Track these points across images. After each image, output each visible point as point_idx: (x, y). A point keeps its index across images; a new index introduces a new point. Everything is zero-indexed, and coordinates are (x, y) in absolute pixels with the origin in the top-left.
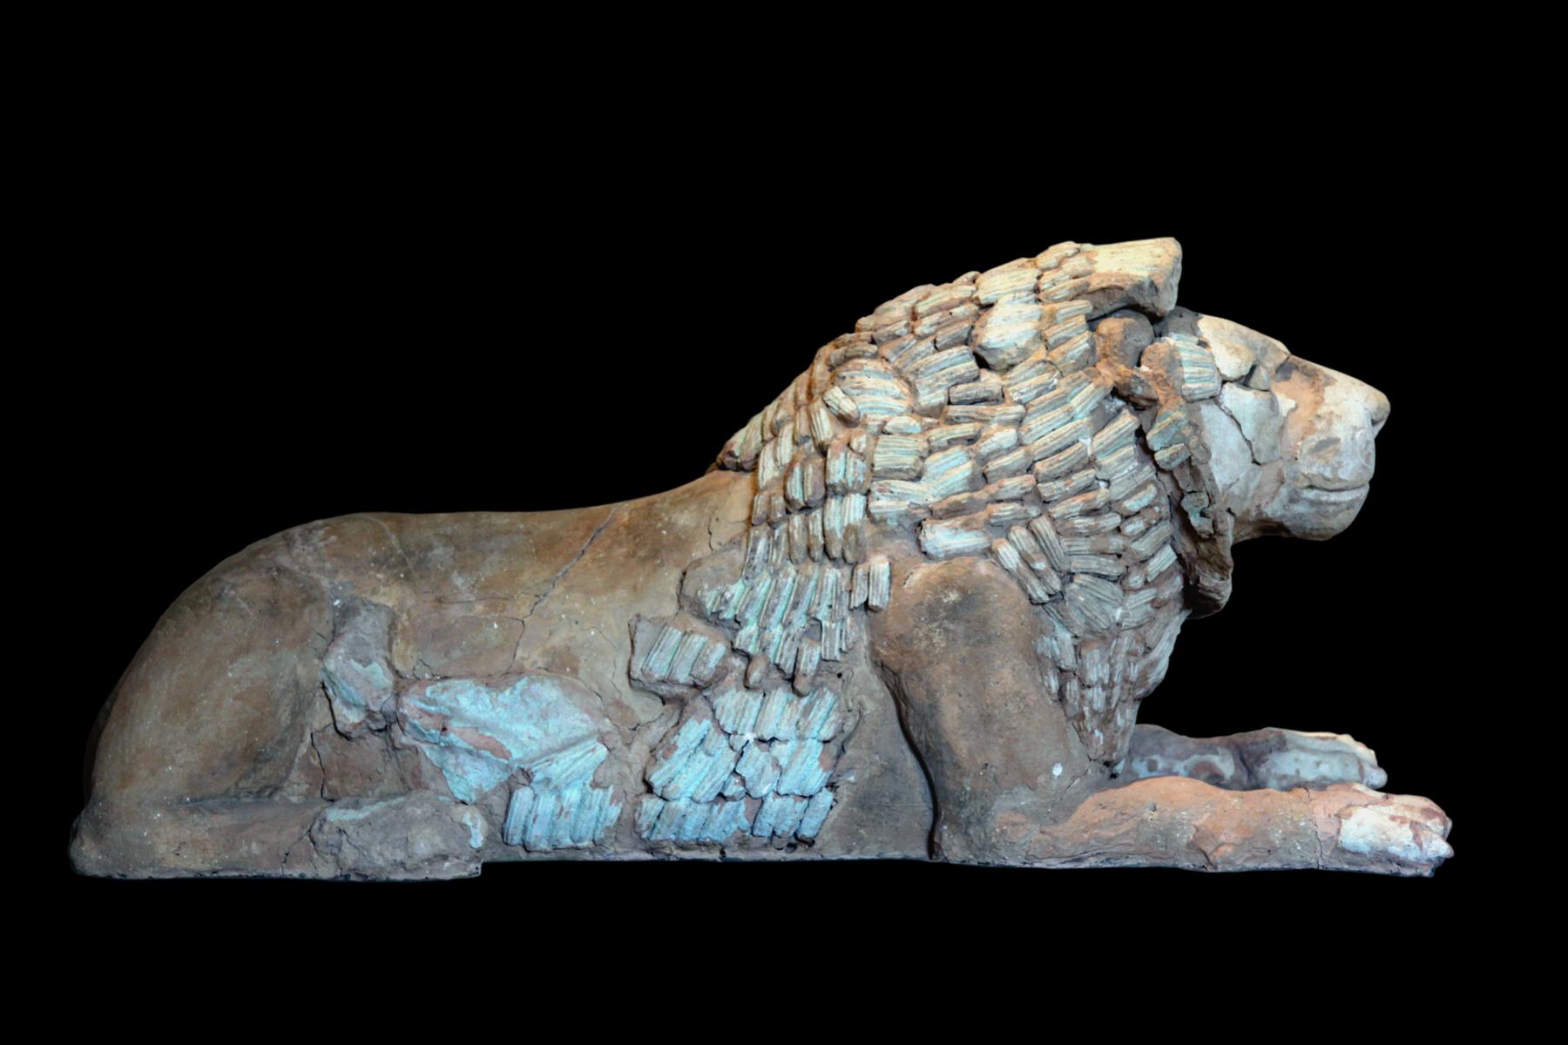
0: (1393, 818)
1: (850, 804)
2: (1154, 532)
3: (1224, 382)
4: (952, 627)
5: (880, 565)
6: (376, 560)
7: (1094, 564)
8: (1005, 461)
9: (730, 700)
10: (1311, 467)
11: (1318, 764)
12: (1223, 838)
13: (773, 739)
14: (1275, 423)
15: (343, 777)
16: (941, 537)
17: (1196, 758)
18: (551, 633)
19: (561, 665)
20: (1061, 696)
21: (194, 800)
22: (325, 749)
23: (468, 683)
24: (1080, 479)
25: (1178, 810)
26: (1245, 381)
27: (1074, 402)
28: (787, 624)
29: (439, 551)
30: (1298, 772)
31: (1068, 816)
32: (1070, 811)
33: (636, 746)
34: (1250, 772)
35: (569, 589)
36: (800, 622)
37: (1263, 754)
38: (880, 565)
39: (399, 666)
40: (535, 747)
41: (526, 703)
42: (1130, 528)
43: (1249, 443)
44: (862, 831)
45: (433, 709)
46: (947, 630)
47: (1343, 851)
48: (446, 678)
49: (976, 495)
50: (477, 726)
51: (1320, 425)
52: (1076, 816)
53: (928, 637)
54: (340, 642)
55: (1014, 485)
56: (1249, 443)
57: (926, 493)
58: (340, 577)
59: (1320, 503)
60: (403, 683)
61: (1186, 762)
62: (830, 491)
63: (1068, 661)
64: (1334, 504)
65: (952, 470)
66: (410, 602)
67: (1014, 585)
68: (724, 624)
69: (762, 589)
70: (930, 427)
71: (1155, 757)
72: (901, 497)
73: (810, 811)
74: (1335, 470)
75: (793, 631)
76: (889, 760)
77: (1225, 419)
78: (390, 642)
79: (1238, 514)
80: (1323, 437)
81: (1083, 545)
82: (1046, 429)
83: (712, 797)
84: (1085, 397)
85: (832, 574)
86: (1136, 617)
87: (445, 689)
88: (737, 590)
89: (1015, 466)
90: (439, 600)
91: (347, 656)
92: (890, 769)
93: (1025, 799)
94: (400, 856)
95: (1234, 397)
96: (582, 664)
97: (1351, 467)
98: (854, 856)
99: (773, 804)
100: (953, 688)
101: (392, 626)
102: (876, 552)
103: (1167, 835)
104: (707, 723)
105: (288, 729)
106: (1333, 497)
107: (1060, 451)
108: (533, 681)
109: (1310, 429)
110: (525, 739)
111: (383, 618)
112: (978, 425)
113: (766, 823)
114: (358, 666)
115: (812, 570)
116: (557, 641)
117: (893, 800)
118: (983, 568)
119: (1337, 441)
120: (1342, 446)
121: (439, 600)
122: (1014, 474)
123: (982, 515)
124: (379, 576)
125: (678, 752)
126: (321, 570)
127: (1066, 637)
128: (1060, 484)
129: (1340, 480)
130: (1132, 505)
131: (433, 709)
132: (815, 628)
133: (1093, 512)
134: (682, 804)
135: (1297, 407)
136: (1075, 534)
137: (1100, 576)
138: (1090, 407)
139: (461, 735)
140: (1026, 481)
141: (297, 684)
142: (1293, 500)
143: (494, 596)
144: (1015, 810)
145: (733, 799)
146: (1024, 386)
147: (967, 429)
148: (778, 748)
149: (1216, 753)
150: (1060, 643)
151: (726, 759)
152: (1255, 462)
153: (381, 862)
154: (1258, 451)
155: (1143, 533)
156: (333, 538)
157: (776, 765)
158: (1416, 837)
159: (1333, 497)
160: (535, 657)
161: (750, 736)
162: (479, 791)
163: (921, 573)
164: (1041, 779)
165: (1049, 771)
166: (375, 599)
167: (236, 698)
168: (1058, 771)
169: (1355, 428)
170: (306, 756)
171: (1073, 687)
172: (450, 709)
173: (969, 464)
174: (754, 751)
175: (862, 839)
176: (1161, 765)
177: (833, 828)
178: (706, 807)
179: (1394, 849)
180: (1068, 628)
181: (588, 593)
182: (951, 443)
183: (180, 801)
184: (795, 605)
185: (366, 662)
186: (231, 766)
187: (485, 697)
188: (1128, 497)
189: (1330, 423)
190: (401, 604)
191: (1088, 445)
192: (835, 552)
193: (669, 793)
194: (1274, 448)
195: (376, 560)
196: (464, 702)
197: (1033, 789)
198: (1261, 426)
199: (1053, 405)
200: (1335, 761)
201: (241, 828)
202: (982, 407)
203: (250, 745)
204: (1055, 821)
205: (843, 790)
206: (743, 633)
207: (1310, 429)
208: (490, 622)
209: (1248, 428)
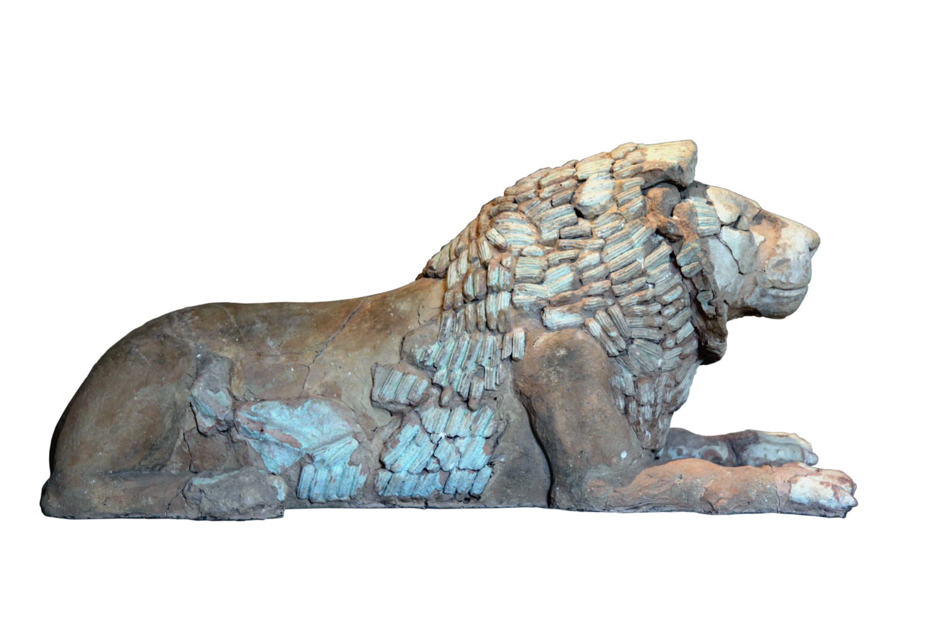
0: (822, 483)
1: (502, 475)
2: (681, 314)
3: (722, 226)
4: (561, 370)
5: (519, 334)
6: (222, 331)
7: (645, 333)
8: (593, 272)
9: (431, 413)
10: (773, 276)
11: (778, 451)
12: (721, 495)
13: (456, 436)
14: (752, 250)
15: (202, 459)
16: (555, 317)
17: (705, 448)
18: (325, 374)
19: (331, 393)
20: (626, 411)
21: (114, 472)
22: (192, 442)
23: (276, 403)
24: (637, 283)
25: (695, 478)
26: (734, 225)
27: (634, 237)
28: (464, 369)
29: (259, 325)
30: (766, 456)
31: (630, 482)
32: (631, 479)
33: (375, 441)
34: (738, 456)
35: (336, 348)
36: (472, 367)
37: (745, 445)
38: (519, 334)
39: (235, 393)
40: (316, 441)
41: (310, 415)
42: (666, 312)
43: (737, 261)
44: (509, 491)
45: (255, 418)
46: (558, 372)
47: (793, 502)
48: (263, 400)
49: (576, 292)
50: (281, 429)
51: (779, 251)
52: (635, 482)
53: (547, 376)
54: (201, 379)
55: (598, 286)
56: (737, 261)
57: (546, 291)
58: (201, 341)
59: (779, 297)
60: (238, 403)
61: (700, 450)
62: (490, 290)
63: (630, 390)
64: (787, 297)
65: (562, 277)
66: (242, 355)
67: (598, 346)
68: (427, 368)
69: (450, 348)
70: (548, 252)
71: (682, 447)
72: (532, 293)
73: (478, 479)
74: (787, 278)
75: (468, 373)
76: (524, 449)
77: (723, 247)
78: (230, 379)
79: (730, 304)
80: (780, 258)
81: (639, 322)
82: (617, 253)
83: (420, 471)
84: (640, 234)
85: (491, 339)
86: (670, 364)
87: (262, 407)
88: (435, 348)
89: (599, 275)
90: (259, 354)
91: (205, 388)
92: (525, 454)
93: (605, 472)
94: (236, 505)
95: (728, 235)
96: (343, 392)
97: (797, 276)
99: (456, 475)
100: (562, 406)
101: (231, 370)
102: (517, 326)
103: (688, 493)
104: (417, 427)
105: (170, 430)
106: (787, 294)
107: (625, 266)
108: (314, 402)
109: (773, 254)
110: (310, 436)
111: (226, 365)
112: (577, 251)
113: (452, 486)
114: (211, 393)
115: (479, 336)
116: (329, 378)
117: (527, 472)
118: (580, 335)
119: (789, 260)
120: (792, 263)
121: (259, 354)
122: (598, 280)
123: (579, 304)
124: (224, 340)
125: (400, 444)
126: (189, 336)
127: (629, 376)
128: (625, 286)
129: (791, 283)
130: (668, 298)
131: (255, 418)
132: (481, 371)
133: (644, 302)
134: (402, 474)
135: (765, 240)
136: (634, 315)
137: (649, 340)
138: (643, 240)
139: (272, 434)
140: (605, 284)
141: (175, 404)
142: (763, 295)
143: (292, 352)
144: (599, 478)
145: (432, 471)
146: (604, 228)
147: (570, 253)
148: (459, 442)
149: (718, 445)
150: (626, 380)
151: (428, 448)
152: (740, 273)
153: (224, 509)
154: (742, 266)
155: (674, 315)
156: (197, 318)
157: (458, 451)
158: (835, 494)
159: (787, 294)
160: (315, 388)
161: (442, 435)
162: (283, 467)
163: (543, 339)
164: (614, 460)
165: (619, 455)
166: (221, 354)
167: (139, 412)
168: (624, 455)
169: (799, 253)
170: (180, 447)
171: (633, 405)
172: (266, 418)
173: (572, 274)
174: (445, 444)
175: (508, 495)
176: (685, 452)
177: (491, 489)
178: (416, 477)
179: (822, 502)
180: (630, 371)
181: (347, 350)
182: (561, 261)
183: (106, 473)
184: (469, 357)
185: (216, 391)
186: (136, 452)
187: (286, 411)
188: (665, 293)
189: (784, 250)
190: (237, 356)
191: (642, 263)
192: (493, 326)
193: (395, 468)
194: (752, 264)
195: (222, 331)
196: (274, 414)
197: (609, 466)
198: (744, 252)
199: (621, 239)
200: (788, 449)
201: (142, 489)
202: (579, 241)
203: (148, 440)
204: (622, 485)
205: (497, 466)
206: (438, 374)
207: (773, 254)
208: (289, 367)
209: (736, 253)
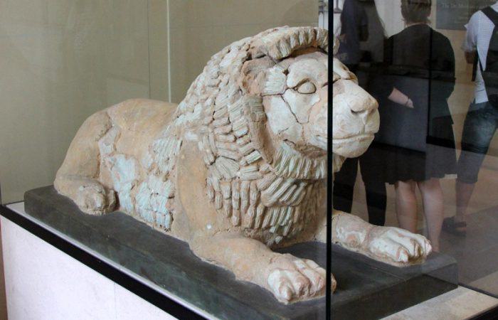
2: (248, 145)
7: (226, 154)
11: (386, 246)
14: (307, 107)
17: (353, 232)
24: (225, 120)
26: (295, 89)
29: (138, 114)
37: (375, 237)
39: (117, 147)
42: (239, 141)
43: (294, 115)
63: (216, 188)
65: (198, 108)
69: (163, 142)
81: (222, 145)
84: (232, 89)
86: (248, 176)
88: (159, 141)
95: (290, 96)
98: (179, 238)
99: (157, 214)
130: (238, 134)
131: (113, 162)
133: (227, 134)
141: (89, 148)
149: (361, 232)
158: (280, 288)
164: (204, 229)
165: (205, 226)
168: (209, 227)
171: (218, 198)
176: (343, 232)
178: (248, 182)
185: (107, 145)
197: (203, 230)
